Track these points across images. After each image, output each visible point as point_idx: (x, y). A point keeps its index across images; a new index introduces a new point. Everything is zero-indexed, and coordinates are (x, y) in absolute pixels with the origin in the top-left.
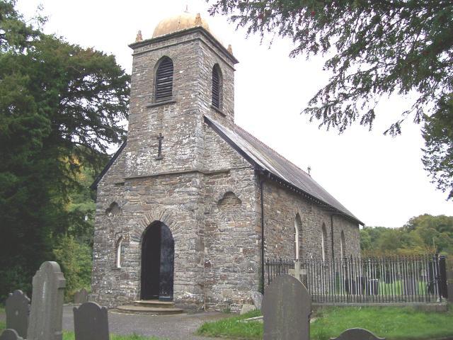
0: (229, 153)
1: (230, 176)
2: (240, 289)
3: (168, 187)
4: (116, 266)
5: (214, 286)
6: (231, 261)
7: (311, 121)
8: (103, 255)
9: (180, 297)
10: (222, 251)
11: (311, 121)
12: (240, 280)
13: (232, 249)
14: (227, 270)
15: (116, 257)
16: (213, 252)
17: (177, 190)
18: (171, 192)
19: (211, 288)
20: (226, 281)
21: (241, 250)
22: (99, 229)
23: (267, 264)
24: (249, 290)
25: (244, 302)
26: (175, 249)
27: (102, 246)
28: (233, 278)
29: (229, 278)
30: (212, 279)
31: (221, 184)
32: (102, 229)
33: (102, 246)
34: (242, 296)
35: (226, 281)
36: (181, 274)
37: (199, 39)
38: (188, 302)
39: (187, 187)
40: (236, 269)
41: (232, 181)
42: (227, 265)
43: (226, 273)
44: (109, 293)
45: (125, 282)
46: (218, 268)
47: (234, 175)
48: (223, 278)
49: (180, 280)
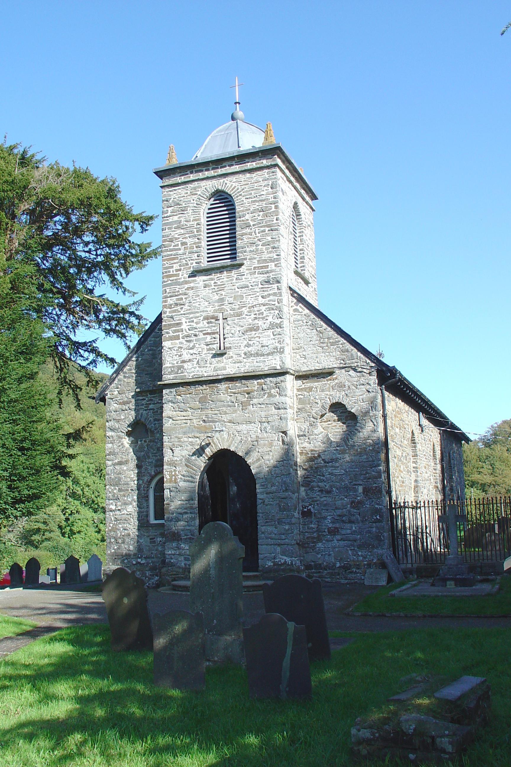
0: (332, 344)
1: (336, 378)
2: (360, 547)
3: (240, 397)
4: (148, 521)
5: (320, 545)
6: (344, 507)
7: (502, 34)
8: (125, 504)
9: (270, 564)
10: (329, 492)
11: (502, 34)
12: (360, 533)
13: (347, 489)
14: (340, 520)
15: (148, 507)
16: (316, 495)
17: (255, 401)
18: (244, 405)
19: (314, 548)
20: (339, 537)
21: (360, 489)
22: (114, 465)
23: (223, 199)
24: (373, 547)
25: (369, 565)
26: (258, 491)
27: (120, 490)
28: (349, 531)
29: (344, 532)
30: (315, 535)
31: (323, 391)
32: (120, 463)
33: (120, 490)
34: (365, 557)
35: (339, 537)
36: (269, 529)
37: (276, 165)
38: (283, 570)
39: (270, 395)
40: (353, 518)
41: (341, 386)
42: (339, 512)
43: (337, 525)
44: (139, 563)
45: (174, 544)
46: (325, 518)
47: (341, 376)
48: (333, 532)
49: (267, 538)
